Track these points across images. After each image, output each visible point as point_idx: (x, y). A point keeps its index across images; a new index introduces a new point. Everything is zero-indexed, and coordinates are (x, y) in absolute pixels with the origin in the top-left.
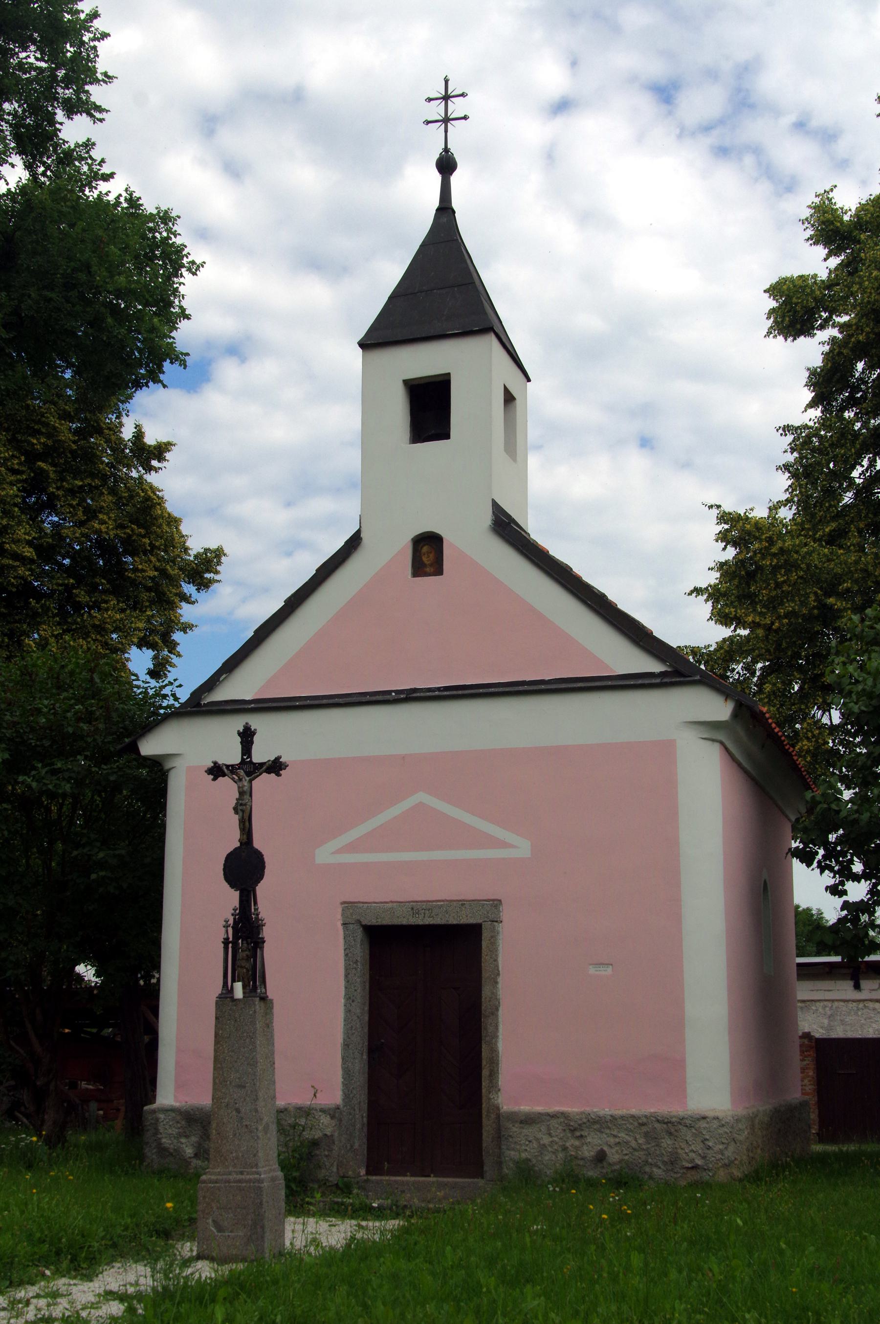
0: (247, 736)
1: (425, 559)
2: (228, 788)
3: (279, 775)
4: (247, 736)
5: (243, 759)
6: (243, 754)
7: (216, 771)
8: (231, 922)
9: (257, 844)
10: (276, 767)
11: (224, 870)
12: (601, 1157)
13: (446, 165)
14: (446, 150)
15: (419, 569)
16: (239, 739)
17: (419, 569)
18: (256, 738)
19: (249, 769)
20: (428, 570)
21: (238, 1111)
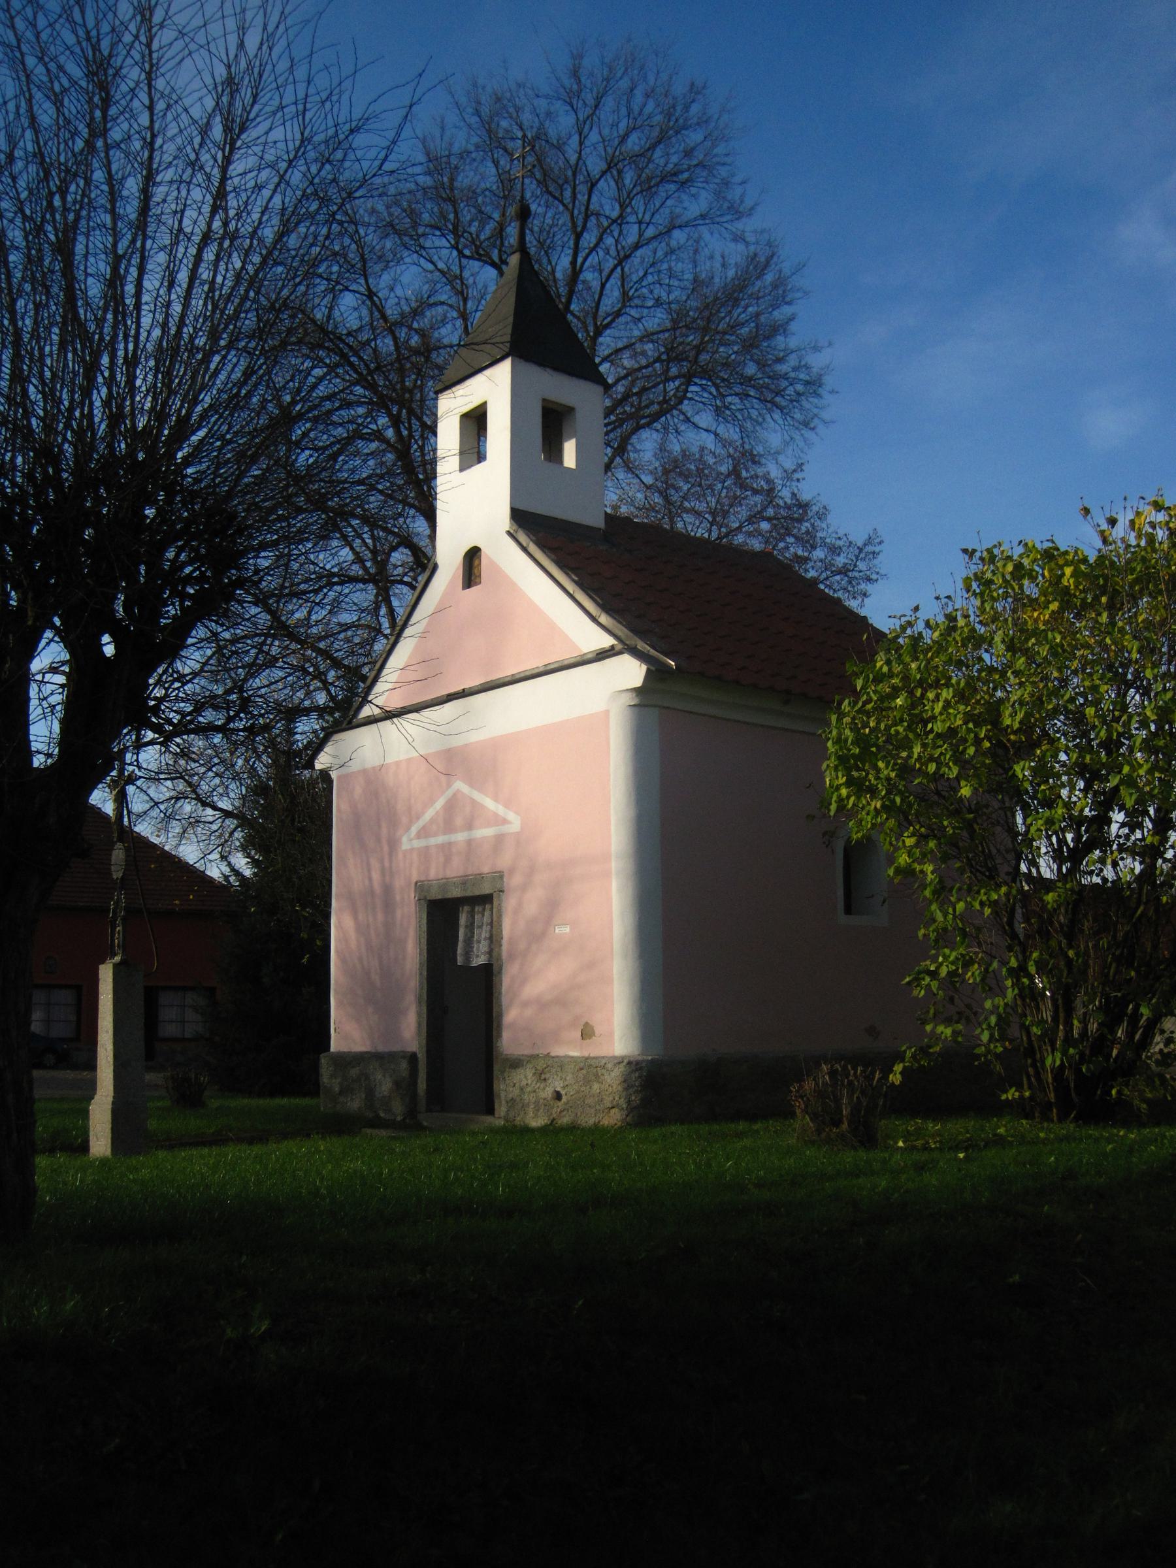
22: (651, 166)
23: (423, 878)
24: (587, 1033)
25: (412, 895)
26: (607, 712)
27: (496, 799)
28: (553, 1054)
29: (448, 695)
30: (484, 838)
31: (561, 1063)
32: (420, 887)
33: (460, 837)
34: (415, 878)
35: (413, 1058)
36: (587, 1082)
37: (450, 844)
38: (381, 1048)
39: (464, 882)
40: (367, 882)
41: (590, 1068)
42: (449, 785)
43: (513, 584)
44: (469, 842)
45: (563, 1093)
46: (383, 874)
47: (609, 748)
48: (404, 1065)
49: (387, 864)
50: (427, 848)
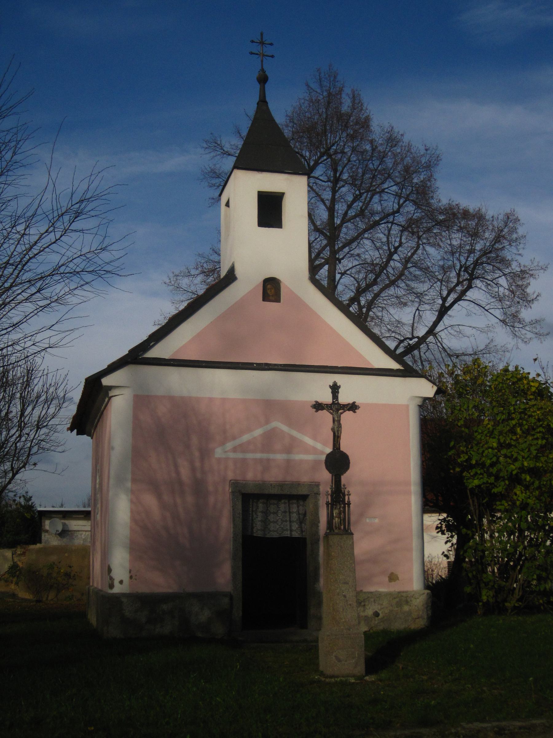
0: (335, 389)
1: (269, 292)
2: (326, 417)
3: (355, 412)
4: (335, 389)
5: (333, 402)
6: (333, 399)
7: (318, 406)
8: (330, 492)
9: (343, 448)
10: (353, 407)
11: (349, 461)
12: (376, 614)
13: (263, 80)
14: (263, 70)
15: (266, 297)
16: (330, 390)
17: (266, 297)
18: (340, 390)
19: (336, 408)
20: (271, 298)
21: (345, 596)
22: (403, 148)
23: (239, 478)
24: (393, 578)
25: (228, 489)
26: (407, 406)
27: (315, 438)
28: (364, 590)
29: (267, 364)
30: (301, 461)
31: (377, 597)
32: (235, 484)
33: (280, 457)
34: (230, 475)
35: (231, 597)
36: (399, 604)
37: (268, 460)
38: (190, 589)
39: (281, 485)
40: (174, 475)
41: (402, 599)
42: (267, 422)
43: (319, 317)
44: (288, 461)
45: (380, 612)
46: (193, 470)
47: (409, 425)
48: (226, 600)
49: (198, 464)
50: (244, 460)
